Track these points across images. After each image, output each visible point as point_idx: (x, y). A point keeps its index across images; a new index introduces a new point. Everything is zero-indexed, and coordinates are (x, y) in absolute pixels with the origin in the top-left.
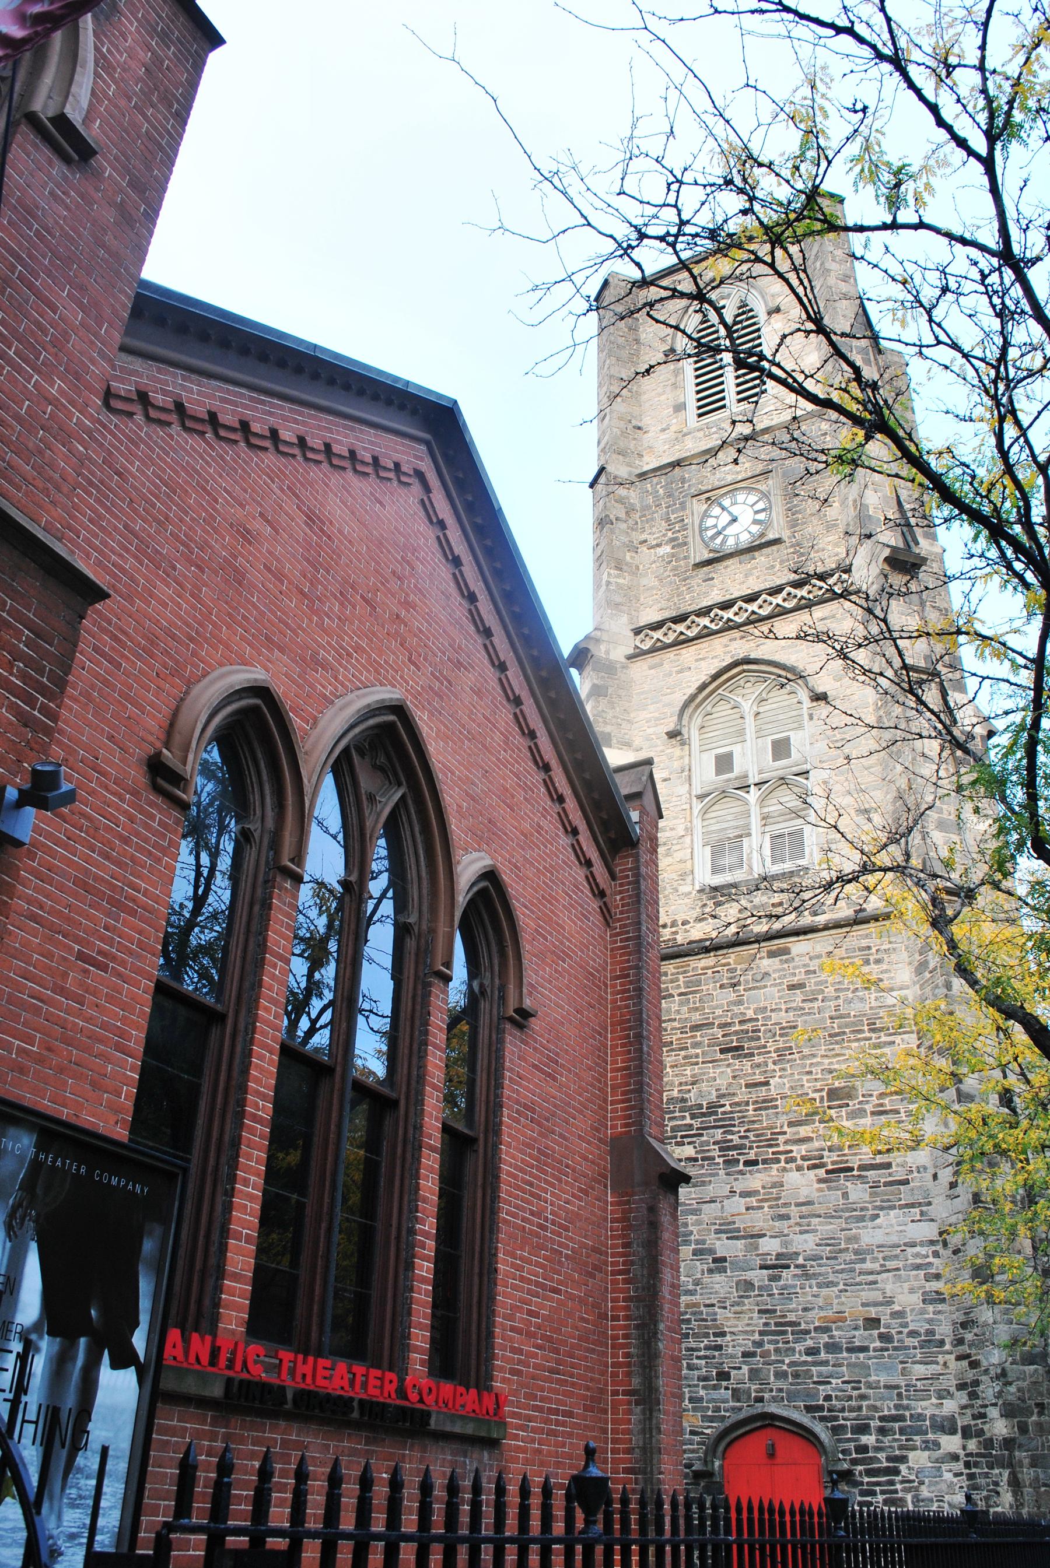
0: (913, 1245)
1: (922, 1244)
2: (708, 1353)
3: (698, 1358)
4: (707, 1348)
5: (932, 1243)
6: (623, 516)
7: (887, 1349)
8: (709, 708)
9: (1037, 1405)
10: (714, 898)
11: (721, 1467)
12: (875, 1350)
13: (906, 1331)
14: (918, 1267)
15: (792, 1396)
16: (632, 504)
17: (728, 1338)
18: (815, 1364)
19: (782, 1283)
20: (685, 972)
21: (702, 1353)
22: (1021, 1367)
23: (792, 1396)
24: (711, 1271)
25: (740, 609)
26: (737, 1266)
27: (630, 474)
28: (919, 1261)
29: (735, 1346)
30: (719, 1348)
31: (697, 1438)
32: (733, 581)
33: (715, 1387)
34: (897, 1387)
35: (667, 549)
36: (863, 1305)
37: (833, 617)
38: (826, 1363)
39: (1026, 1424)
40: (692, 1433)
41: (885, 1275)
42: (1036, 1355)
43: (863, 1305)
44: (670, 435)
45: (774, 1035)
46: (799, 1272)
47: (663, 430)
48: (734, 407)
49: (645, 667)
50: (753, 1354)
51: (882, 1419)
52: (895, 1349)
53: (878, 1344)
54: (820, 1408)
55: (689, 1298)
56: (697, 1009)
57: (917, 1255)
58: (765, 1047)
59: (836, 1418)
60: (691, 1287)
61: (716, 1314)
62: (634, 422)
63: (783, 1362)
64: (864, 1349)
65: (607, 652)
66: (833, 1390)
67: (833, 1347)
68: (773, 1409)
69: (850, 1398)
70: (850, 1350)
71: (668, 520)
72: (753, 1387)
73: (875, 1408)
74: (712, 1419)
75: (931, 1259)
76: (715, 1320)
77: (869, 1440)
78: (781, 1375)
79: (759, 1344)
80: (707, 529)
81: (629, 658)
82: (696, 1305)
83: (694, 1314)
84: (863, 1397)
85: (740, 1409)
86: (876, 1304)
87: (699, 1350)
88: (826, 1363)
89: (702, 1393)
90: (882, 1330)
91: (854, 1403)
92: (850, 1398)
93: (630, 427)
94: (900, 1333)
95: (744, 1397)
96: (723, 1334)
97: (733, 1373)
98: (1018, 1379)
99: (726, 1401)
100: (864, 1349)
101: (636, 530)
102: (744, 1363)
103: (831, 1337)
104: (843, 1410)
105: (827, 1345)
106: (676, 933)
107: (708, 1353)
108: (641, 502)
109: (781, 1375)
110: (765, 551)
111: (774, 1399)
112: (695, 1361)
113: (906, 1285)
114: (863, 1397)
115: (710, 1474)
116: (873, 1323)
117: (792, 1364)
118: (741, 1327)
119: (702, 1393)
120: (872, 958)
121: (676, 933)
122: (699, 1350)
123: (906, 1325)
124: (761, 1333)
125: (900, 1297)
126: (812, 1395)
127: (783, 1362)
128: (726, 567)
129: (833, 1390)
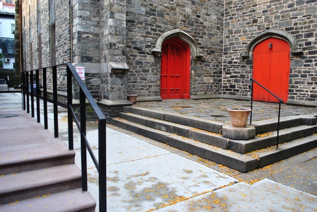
2: (250, 13)
3: (247, 16)
4: (250, 12)
11: (252, 54)
15: (280, 25)
17: (258, 6)
18: (291, 11)
30: (254, 11)
31: (245, 45)
33: (252, 26)
38: (296, 9)
50: (267, 11)
54: (292, 28)
59: (298, 32)
63: (278, 12)
66: (298, 20)
72: (266, 24)
79: (269, 7)
88: (296, 9)
89: (247, 28)
91: (307, 25)
95: (262, 28)
96: (256, 5)
97: (259, 19)
102: (263, 15)
104: (302, 28)
107: (250, 13)
112: (246, 17)
117: (282, 12)
119: (247, 28)
127: (278, 12)
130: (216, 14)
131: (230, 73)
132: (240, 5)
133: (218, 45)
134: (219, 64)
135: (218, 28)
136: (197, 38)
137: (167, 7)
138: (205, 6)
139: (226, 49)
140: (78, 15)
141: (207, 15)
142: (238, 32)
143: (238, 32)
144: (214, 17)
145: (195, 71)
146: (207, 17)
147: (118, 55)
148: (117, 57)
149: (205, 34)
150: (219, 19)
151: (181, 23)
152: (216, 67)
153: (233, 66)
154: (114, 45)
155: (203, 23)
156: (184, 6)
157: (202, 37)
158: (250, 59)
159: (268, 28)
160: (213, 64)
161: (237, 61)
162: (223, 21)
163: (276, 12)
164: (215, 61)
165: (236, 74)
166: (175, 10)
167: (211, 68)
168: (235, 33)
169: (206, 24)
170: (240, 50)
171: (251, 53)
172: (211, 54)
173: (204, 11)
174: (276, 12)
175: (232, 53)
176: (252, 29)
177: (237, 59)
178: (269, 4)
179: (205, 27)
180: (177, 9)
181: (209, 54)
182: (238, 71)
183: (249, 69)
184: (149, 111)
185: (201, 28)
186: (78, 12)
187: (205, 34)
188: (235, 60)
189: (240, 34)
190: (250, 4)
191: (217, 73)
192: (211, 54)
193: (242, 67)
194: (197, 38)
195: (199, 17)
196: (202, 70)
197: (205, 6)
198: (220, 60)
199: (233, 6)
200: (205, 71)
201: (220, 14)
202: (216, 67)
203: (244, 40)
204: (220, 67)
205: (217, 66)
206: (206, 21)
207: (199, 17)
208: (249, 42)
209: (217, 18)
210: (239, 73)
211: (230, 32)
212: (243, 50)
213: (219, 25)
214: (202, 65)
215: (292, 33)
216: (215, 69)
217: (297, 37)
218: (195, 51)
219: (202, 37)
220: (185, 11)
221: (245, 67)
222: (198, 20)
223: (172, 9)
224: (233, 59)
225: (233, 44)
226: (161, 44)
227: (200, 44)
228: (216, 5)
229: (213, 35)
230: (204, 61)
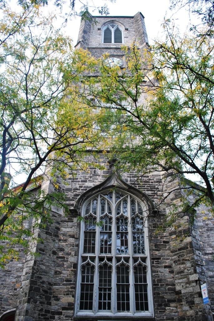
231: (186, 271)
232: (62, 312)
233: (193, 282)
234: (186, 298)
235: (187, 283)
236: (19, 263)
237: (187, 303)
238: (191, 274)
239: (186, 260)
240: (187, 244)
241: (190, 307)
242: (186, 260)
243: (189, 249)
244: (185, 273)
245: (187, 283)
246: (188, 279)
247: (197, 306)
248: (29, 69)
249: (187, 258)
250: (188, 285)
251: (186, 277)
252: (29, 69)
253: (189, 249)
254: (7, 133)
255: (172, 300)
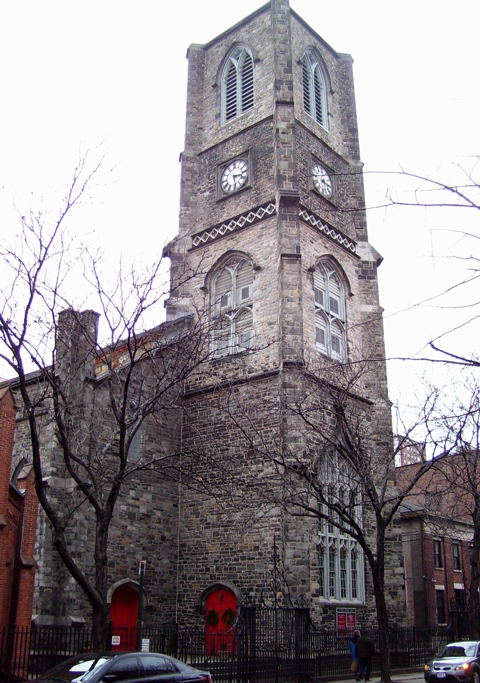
0: (272, 517)
1: (275, 516)
2: (203, 561)
3: (200, 563)
4: (203, 559)
5: (278, 516)
6: (190, 178)
7: (260, 559)
8: (219, 274)
9: (302, 581)
10: (214, 366)
11: (205, 604)
12: (257, 559)
13: (267, 551)
14: (273, 525)
15: (229, 577)
16: (194, 171)
17: (210, 555)
18: (237, 564)
19: (228, 532)
20: (202, 401)
21: (201, 561)
22: (297, 566)
23: (229, 577)
24: (205, 528)
25: (251, 215)
26: (214, 526)
27: (194, 155)
28: (273, 523)
29: (213, 556)
30: (206, 559)
31: (198, 594)
32: (233, 209)
33: (205, 574)
34: (263, 573)
35: (207, 193)
36: (254, 541)
37: (266, 227)
38: (240, 564)
39: (296, 588)
40: (197, 591)
41: (262, 529)
42: (304, 562)
43: (254, 541)
44: (213, 131)
45: (231, 428)
46: (233, 528)
47: (211, 129)
48: (239, 114)
49: (195, 255)
50: (217, 561)
51: (257, 586)
52: (263, 558)
53: (258, 557)
54: (238, 582)
55: (197, 539)
56: (205, 417)
57: (273, 521)
58: (228, 433)
59: (242, 586)
60: (198, 535)
61: (206, 545)
62: (198, 126)
63: (227, 564)
64: (253, 559)
65: (179, 250)
66: (242, 575)
67: (243, 558)
68: (221, 582)
69: (247, 578)
70: (249, 559)
71: (209, 178)
72: (217, 574)
73: (255, 582)
74: (203, 586)
75: (278, 523)
76: (205, 548)
77: (252, 594)
78: (226, 569)
79: (219, 557)
80: (223, 182)
81: (189, 251)
82: (200, 542)
83: (199, 545)
84: (252, 577)
85: (212, 582)
86: (258, 541)
87: (200, 559)
88: (240, 564)
89: (200, 576)
90: (260, 551)
91: (248, 580)
92: (247, 578)
93: (196, 129)
94: (265, 552)
95: (213, 578)
96: (208, 553)
97: (211, 568)
98: (294, 571)
99: (208, 579)
100: (253, 559)
101: (196, 184)
102: (215, 564)
103: (243, 554)
104: (245, 582)
105: (241, 557)
106: (201, 383)
107: (203, 561)
108: (199, 169)
109: (226, 569)
110: (245, 193)
111: (223, 579)
112: (199, 564)
113: (268, 533)
114: (252, 577)
115: (202, 607)
116: (257, 548)
117: (230, 565)
118: (214, 550)
119: (200, 576)
120: (267, 393)
121: (201, 383)
122: (200, 559)
123: (267, 549)
124: (220, 553)
125: (266, 538)
126: (235, 576)
127: (227, 564)
128: (229, 202)
129: (242, 575)
130: (169, 558)
131: (184, 624)
132: (194, 549)
133: (170, 591)
134: (173, 613)
135: (171, 573)
136: (148, 586)
137: (118, 557)
138: (156, 550)
139: (180, 596)
140: (42, 571)
141: (159, 559)
142: (191, 578)
143: (191, 578)
144: (166, 561)
145: (145, 622)
146: (159, 562)
147: (76, 610)
148: (75, 612)
149: (156, 580)
150: (172, 562)
151: (131, 572)
152: (168, 617)
153: (187, 615)
154: (74, 600)
155: (154, 569)
156: (134, 554)
157: (153, 584)
158: (204, 609)
159: (219, 579)
160: (165, 613)
161: (191, 610)
162: (177, 564)
163: (225, 564)
164: (167, 610)
165: (190, 625)
166: (126, 558)
167: (163, 618)
168: (189, 579)
169: (158, 569)
170: (194, 599)
171: (204, 603)
172: (162, 602)
173: (155, 556)
174: (225, 564)
175: (186, 601)
176: (204, 577)
177: (191, 608)
178: (219, 554)
179: (156, 573)
180: (128, 557)
181: (160, 602)
182: (192, 621)
183: (203, 620)
184: (126, 653)
185: (152, 574)
186: (42, 568)
187: (156, 580)
188: (189, 610)
189: (193, 581)
190: (203, 550)
191: (170, 624)
192: (162, 602)
193: (196, 617)
194: (148, 586)
195: (150, 562)
196: (153, 621)
197: (156, 550)
198: (173, 608)
199: (187, 549)
200: (156, 621)
201: (173, 557)
202: (168, 617)
203: (197, 588)
204: (173, 616)
205: (170, 615)
206: (158, 566)
207: (150, 562)
208: (202, 591)
209: (170, 562)
210: (193, 623)
211: (184, 577)
212: (196, 598)
213: (172, 569)
214: (153, 615)
215: (238, 586)
216: (168, 619)
217: (242, 589)
218: (147, 601)
219: (153, 584)
220: (135, 559)
221: (199, 617)
222: (149, 566)
223: (123, 557)
224: (187, 608)
225: (187, 591)
226: (111, 595)
227: (150, 592)
228: (168, 547)
229: (165, 581)
230: (155, 611)
231: (392, 562)
232: (276, 531)
233: (398, 574)
234: (390, 589)
235: (391, 575)
236: (123, 505)
237: (389, 593)
238: (397, 566)
239: (393, 552)
240: (397, 536)
241: (392, 597)
242: (393, 552)
243: (398, 541)
244: (390, 565)
245: (391, 575)
246: (394, 571)
247: (400, 597)
248: (54, 235)
249: (394, 550)
250: (392, 577)
251: (392, 569)
252: (54, 235)
253: (398, 541)
254: (71, 460)
255: (160, 670)
